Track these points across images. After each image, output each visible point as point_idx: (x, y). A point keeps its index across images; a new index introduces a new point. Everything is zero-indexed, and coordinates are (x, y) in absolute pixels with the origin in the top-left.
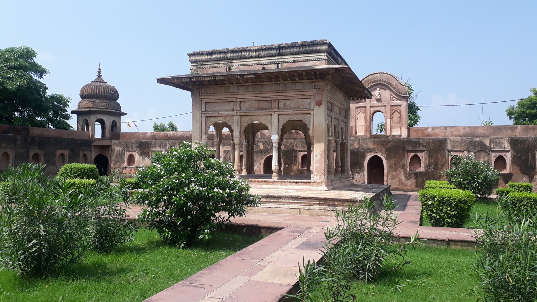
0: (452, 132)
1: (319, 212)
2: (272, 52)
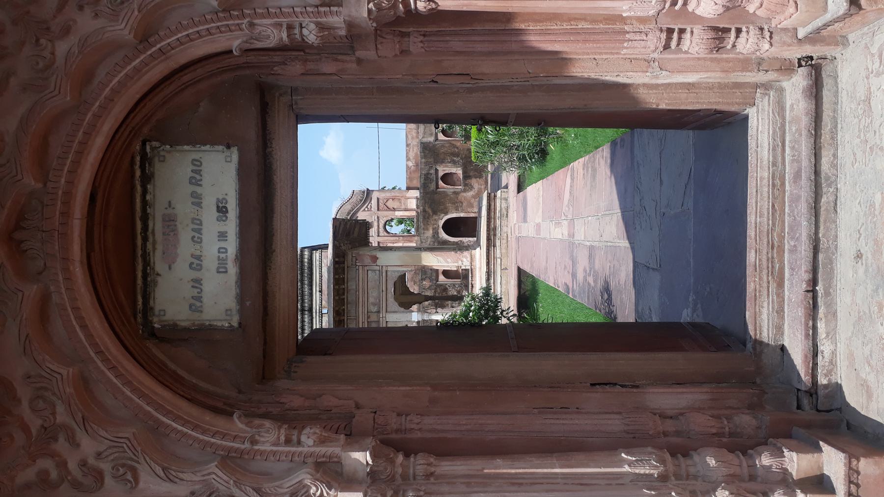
0: (413, 138)
1: (504, 246)
2: (306, 320)
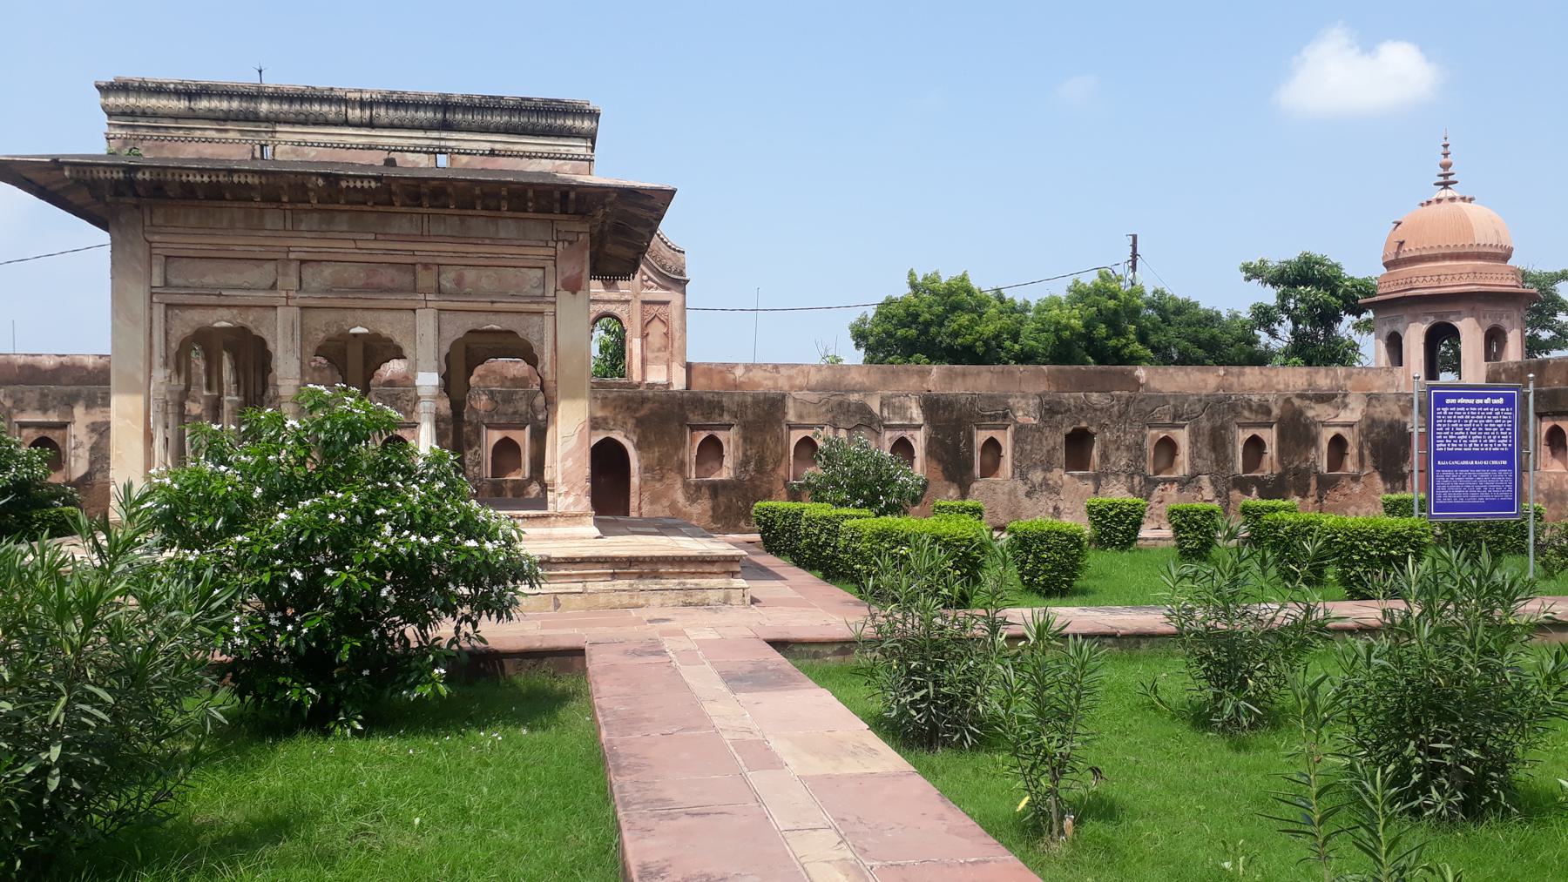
0: (790, 378)
1: (615, 599)
2: (421, 114)
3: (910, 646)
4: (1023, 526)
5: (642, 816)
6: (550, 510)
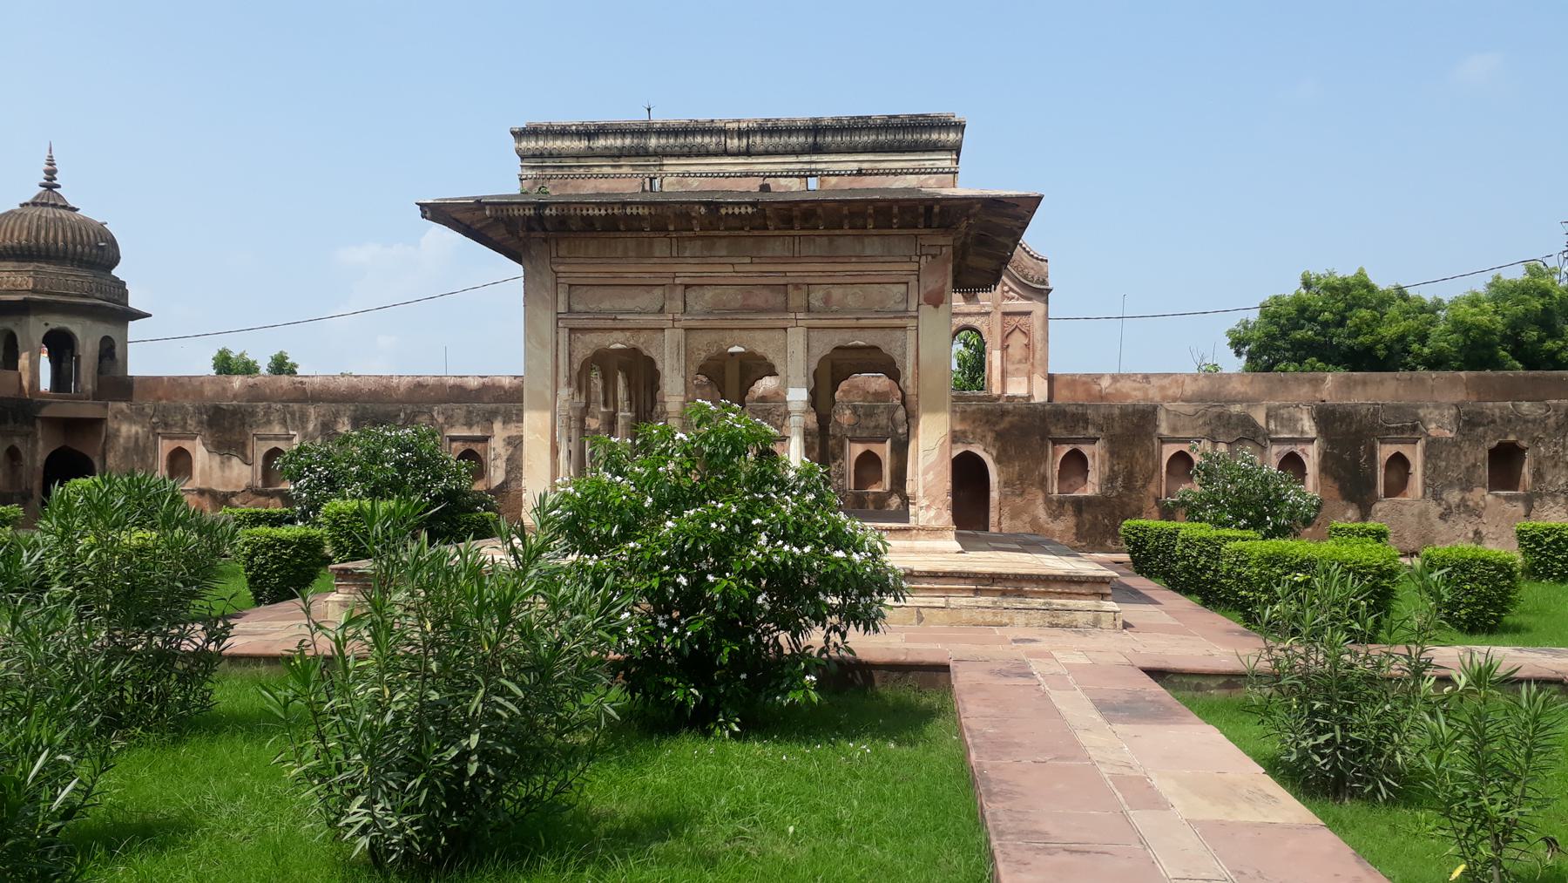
0: (1162, 388)
1: (978, 616)
2: (794, 140)
3: (1310, 684)
4: (1440, 553)
5: (1017, 848)
6: (912, 524)
